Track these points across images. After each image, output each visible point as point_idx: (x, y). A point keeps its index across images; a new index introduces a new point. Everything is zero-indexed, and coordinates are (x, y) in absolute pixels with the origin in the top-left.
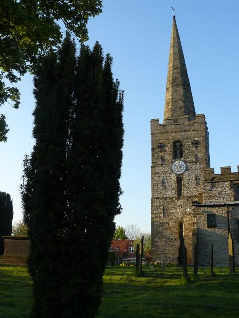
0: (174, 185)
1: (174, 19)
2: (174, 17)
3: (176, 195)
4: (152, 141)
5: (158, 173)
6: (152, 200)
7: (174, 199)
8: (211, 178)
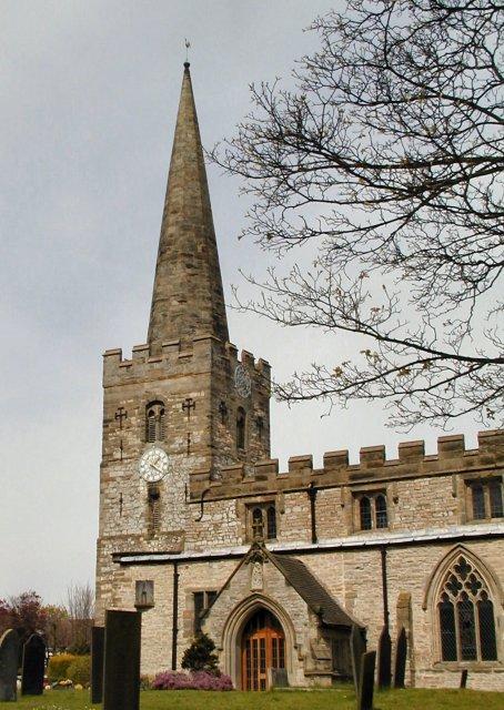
0: (143, 507)
1: (187, 72)
2: (187, 65)
3: (145, 531)
4: (105, 403)
5: (113, 479)
6: (99, 542)
7: (142, 539)
8: (202, 491)
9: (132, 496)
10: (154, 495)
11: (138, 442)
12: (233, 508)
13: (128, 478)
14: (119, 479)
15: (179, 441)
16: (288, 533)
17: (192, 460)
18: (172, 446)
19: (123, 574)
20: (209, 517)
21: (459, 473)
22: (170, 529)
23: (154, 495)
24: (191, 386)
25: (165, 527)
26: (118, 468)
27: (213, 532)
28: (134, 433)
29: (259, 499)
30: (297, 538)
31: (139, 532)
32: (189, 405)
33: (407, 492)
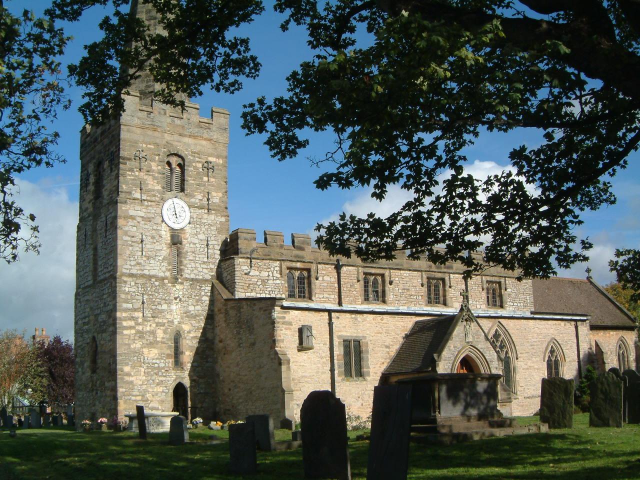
3: (168, 274)
9: (153, 238)
10: (176, 240)
11: (159, 187)
12: (278, 268)
13: (148, 220)
14: (139, 219)
15: (199, 197)
16: (321, 296)
17: (212, 217)
18: (193, 200)
19: (284, 318)
20: (257, 273)
21: (426, 271)
22: (193, 276)
23: (176, 240)
24: (210, 151)
25: (187, 273)
26: (138, 208)
27: (261, 286)
28: (154, 178)
29: (299, 265)
30: (328, 300)
31: (162, 274)
32: (208, 168)
33: (397, 279)
